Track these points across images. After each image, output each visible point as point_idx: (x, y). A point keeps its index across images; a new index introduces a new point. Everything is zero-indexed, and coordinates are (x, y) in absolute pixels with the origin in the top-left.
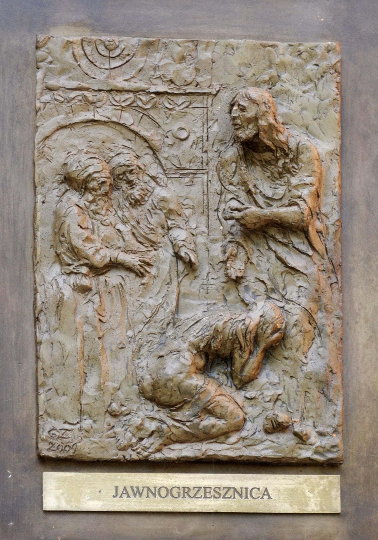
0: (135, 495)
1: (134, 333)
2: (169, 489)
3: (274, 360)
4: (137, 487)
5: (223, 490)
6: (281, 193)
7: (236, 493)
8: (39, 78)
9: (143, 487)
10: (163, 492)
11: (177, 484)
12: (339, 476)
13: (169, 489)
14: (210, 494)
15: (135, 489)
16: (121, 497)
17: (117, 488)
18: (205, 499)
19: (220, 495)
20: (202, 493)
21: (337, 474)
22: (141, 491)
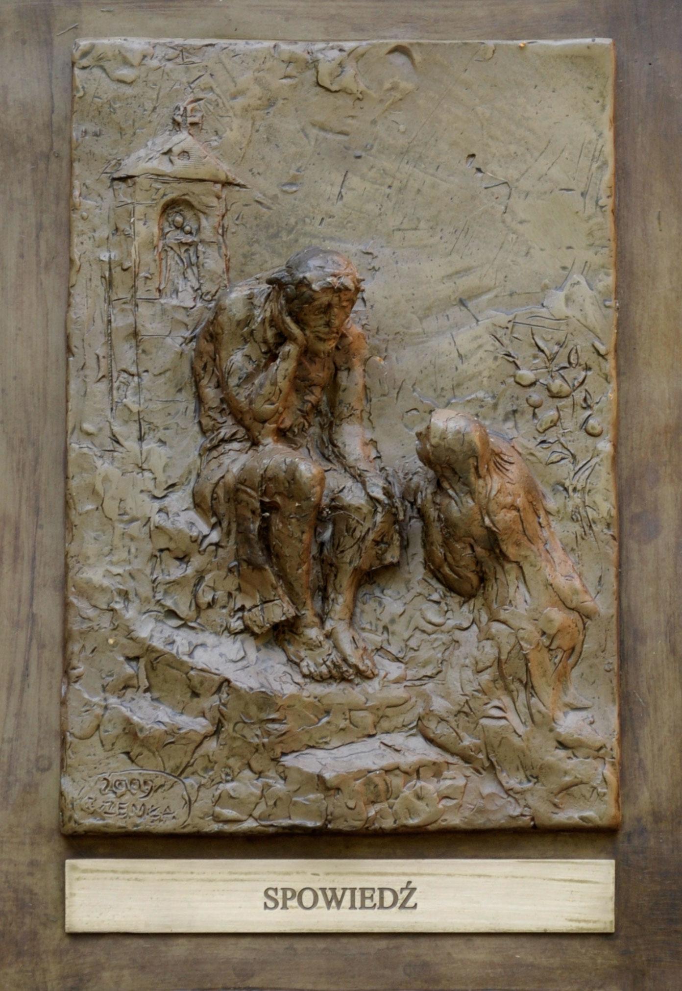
0: (329, 904)
1: (500, 653)
5: (401, 893)
9: (344, 889)
10: (308, 898)
12: (613, 862)
14: (372, 901)
15: (329, 894)
18: (381, 911)
21: (610, 858)
22: (339, 897)
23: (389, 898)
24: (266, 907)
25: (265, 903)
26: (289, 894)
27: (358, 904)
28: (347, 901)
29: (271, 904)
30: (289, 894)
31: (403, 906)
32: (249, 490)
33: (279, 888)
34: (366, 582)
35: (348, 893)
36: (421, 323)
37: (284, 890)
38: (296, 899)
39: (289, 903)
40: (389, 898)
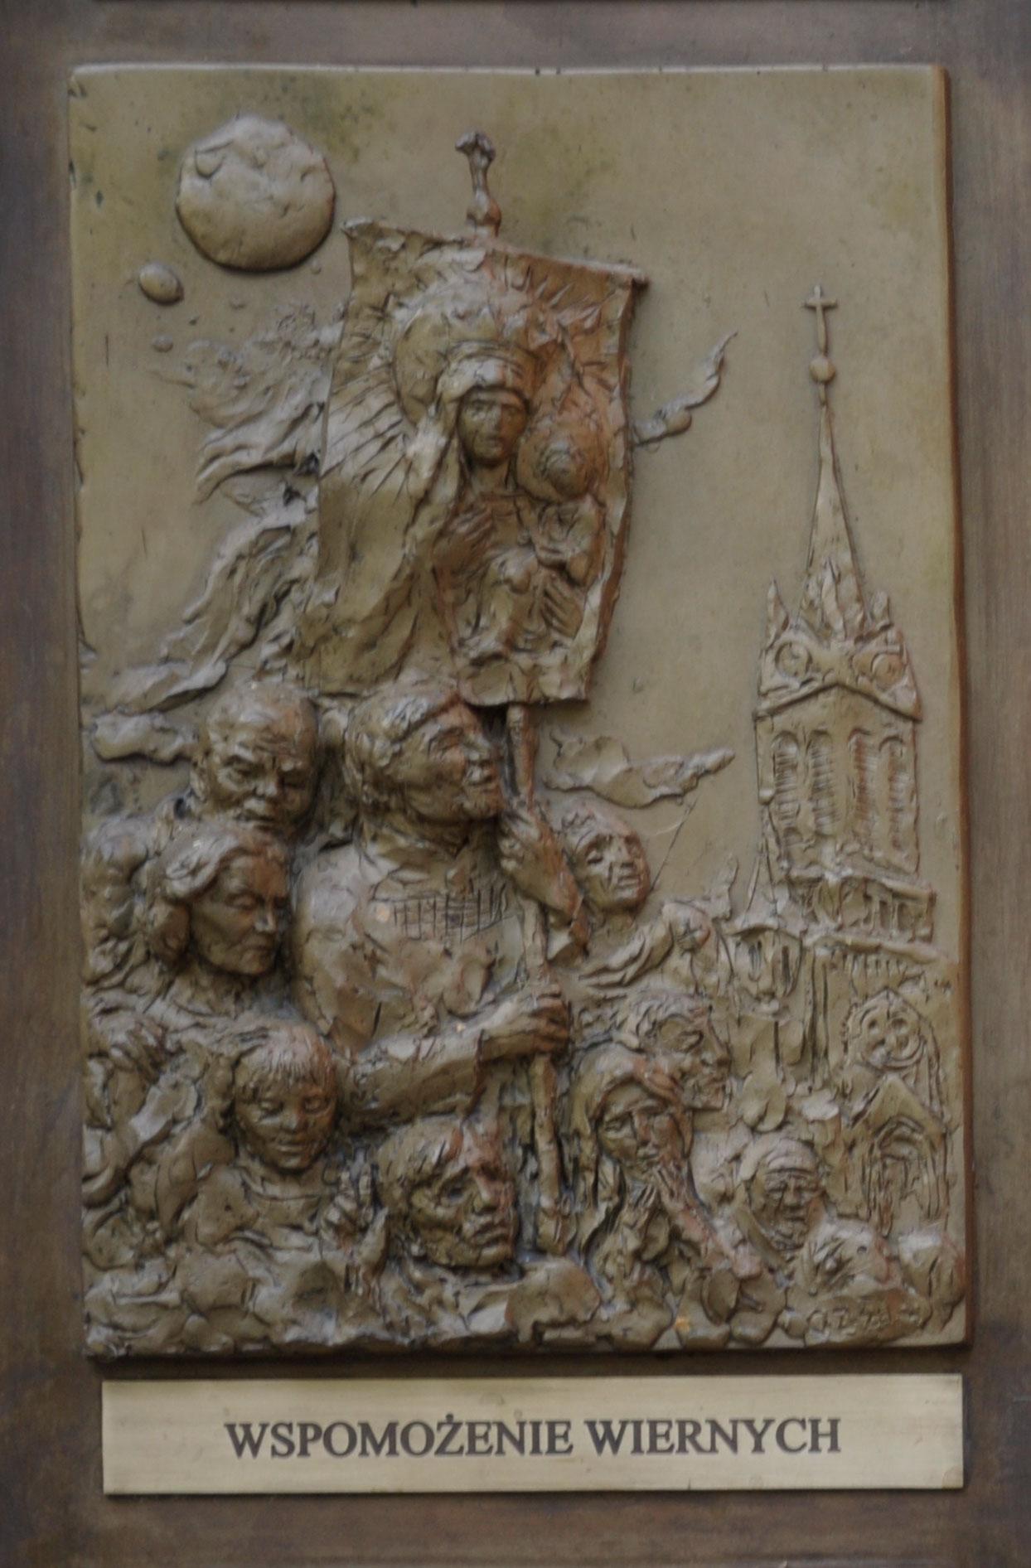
0: (239, 1449)
2: (324, 1428)
3: (850, 1265)
4: (247, 1427)
6: (201, 1169)
7: (517, 1436)
8: (366, 1195)
10: (340, 1439)
11: (657, 1410)
12: (957, 1378)
13: (324, 1428)
15: (600, 1430)
16: (264, 1426)
17: (834, 1447)
19: (291, 1447)
20: (462, 1437)
21: (952, 1371)
22: (616, 1434)
23: (418, 1439)
24: (274, 1452)
25: (273, 1448)
26: (311, 1433)
27: (544, 1444)
28: (627, 1442)
29: (282, 1448)
30: (311, 1433)
31: (441, 1450)
32: (475, 535)
33: (598, 1420)
34: (605, 838)
35: (630, 1429)
36: (353, 288)
37: (304, 1427)
38: (321, 1442)
39: (311, 1447)
40: (418, 1439)
